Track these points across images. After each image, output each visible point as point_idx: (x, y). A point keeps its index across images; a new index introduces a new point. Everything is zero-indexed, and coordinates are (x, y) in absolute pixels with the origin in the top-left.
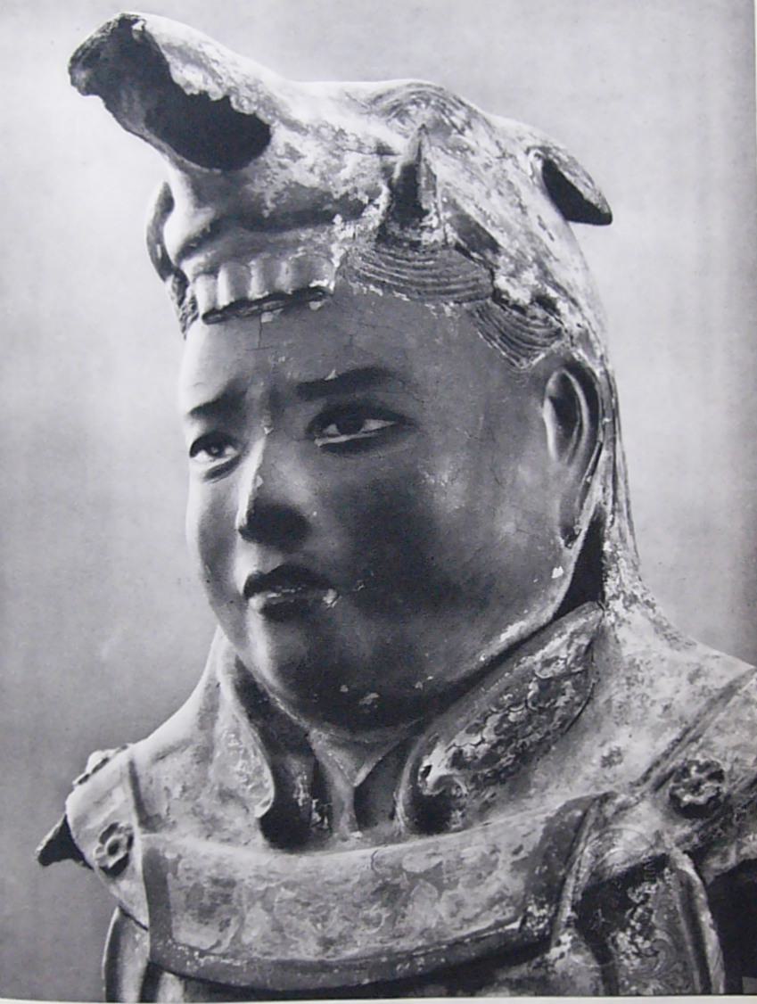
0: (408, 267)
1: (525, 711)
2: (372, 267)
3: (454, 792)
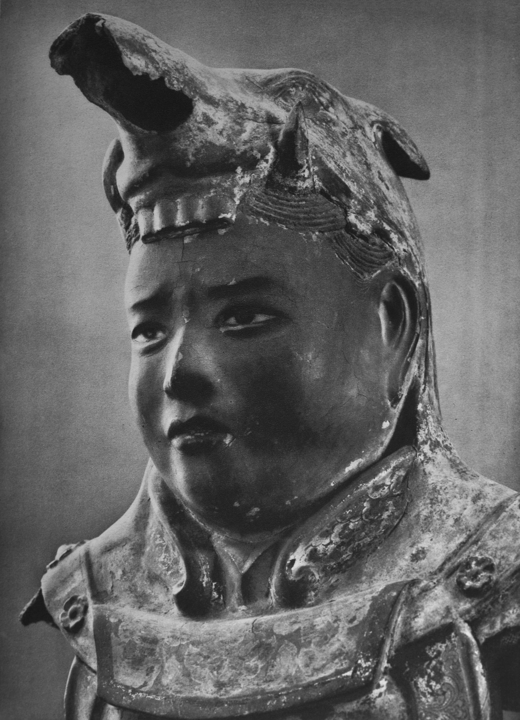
0: (287, 206)
1: (360, 522)
2: (262, 204)
3: (310, 578)
